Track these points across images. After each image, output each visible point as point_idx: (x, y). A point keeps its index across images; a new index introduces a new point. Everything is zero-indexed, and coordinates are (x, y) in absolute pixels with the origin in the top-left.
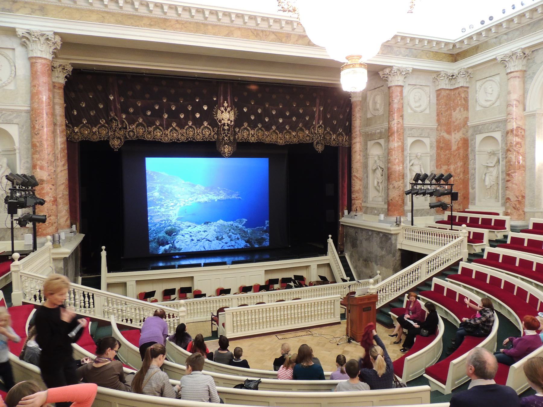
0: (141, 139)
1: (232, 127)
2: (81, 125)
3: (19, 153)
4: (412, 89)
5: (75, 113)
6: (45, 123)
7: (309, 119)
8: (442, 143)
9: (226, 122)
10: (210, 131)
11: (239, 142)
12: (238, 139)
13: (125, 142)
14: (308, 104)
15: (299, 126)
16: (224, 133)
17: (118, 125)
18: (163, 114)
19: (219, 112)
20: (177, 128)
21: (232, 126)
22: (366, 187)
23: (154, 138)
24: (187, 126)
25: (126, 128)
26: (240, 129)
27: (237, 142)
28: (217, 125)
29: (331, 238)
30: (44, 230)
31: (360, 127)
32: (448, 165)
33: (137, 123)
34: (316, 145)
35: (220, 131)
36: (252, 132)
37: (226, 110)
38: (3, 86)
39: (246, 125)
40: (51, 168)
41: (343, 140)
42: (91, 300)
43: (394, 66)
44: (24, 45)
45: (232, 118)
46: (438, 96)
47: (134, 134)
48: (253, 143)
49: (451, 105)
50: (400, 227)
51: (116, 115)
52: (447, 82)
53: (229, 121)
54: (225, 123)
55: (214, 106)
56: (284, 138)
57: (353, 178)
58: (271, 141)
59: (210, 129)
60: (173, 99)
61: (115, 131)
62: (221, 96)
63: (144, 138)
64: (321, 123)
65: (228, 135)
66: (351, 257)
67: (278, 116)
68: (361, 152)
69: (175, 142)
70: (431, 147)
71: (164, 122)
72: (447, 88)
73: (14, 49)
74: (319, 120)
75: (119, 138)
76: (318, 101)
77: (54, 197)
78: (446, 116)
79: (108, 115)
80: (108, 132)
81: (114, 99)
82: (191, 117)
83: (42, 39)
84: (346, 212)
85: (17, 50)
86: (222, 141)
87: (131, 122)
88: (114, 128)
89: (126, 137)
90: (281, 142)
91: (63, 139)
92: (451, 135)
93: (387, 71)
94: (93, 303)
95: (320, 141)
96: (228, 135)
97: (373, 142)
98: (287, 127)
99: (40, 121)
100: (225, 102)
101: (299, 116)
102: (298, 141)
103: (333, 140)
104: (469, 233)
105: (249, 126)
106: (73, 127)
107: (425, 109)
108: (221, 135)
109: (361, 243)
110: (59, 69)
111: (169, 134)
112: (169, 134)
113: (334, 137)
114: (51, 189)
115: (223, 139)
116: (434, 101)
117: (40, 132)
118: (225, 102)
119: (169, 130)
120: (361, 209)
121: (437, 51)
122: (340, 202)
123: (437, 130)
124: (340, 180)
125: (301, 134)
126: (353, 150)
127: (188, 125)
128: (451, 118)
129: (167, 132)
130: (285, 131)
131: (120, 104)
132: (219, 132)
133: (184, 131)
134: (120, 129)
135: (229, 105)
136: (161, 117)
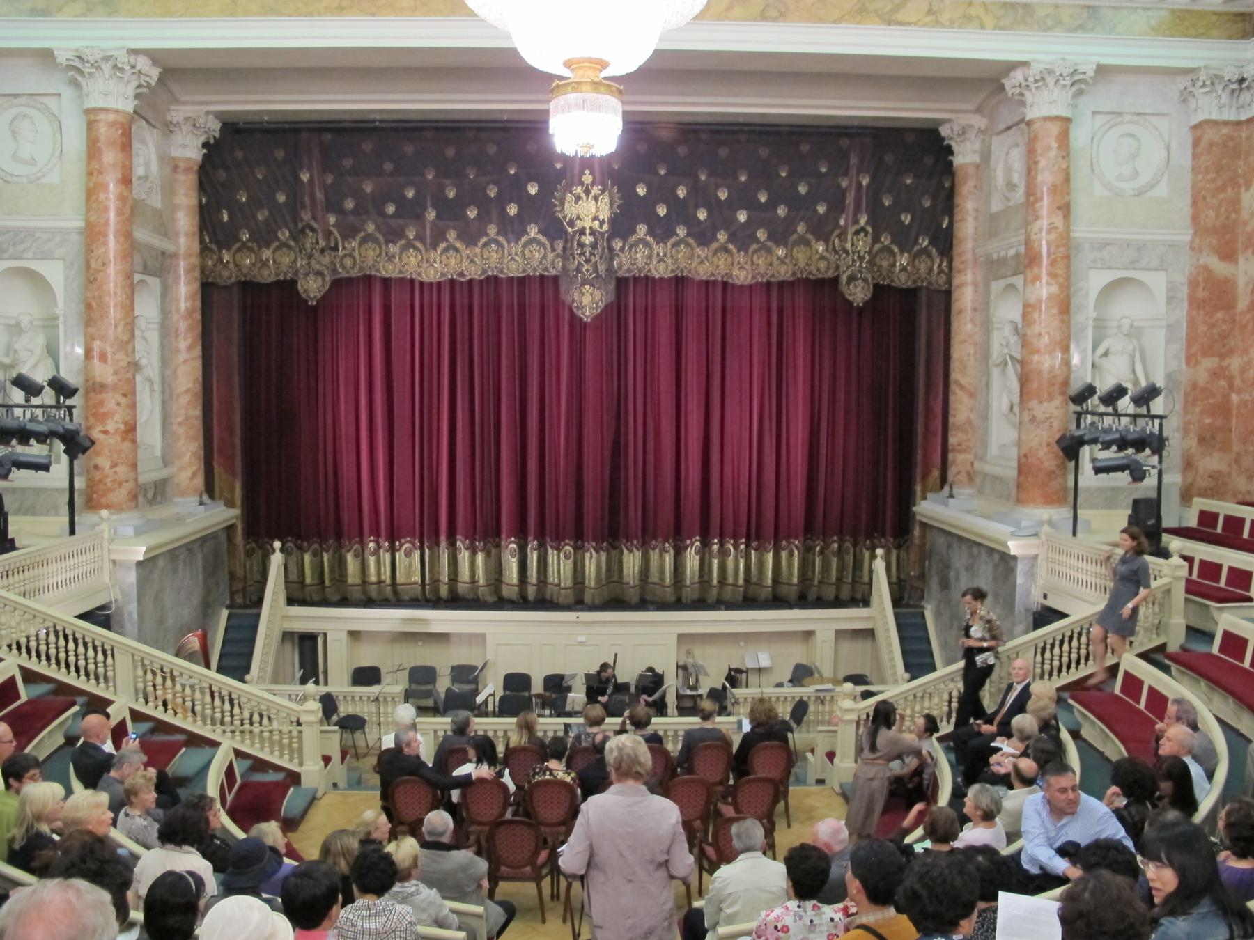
2: (238, 245)
3: (65, 322)
4: (1107, 126)
5: (226, 217)
6: (112, 255)
8: (1201, 288)
10: (545, 249)
12: (620, 268)
15: (795, 231)
17: (317, 242)
18: (425, 208)
20: (458, 245)
21: (602, 234)
23: (400, 272)
25: (336, 249)
30: (103, 495)
32: (1222, 356)
33: (362, 234)
34: (848, 283)
35: (572, 248)
36: (659, 249)
37: (587, 192)
38: (38, 178)
39: (642, 230)
40: (120, 356)
41: (931, 269)
42: (109, 660)
43: (1035, 61)
44: (76, 84)
45: (605, 214)
46: (1196, 143)
47: (355, 263)
48: (661, 279)
49: (1240, 171)
51: (314, 218)
52: (1225, 98)
53: (597, 222)
56: (753, 263)
58: (713, 274)
59: (543, 245)
60: (450, 171)
61: (310, 257)
66: (938, 615)
70: (1170, 299)
71: (428, 231)
72: (1225, 117)
73: (59, 95)
74: (857, 210)
76: (853, 160)
77: (126, 423)
78: (1220, 206)
79: (296, 218)
80: (296, 260)
81: (311, 180)
82: (494, 214)
83: (107, 68)
86: (576, 276)
87: (349, 232)
88: (309, 250)
89: (334, 271)
90: (742, 276)
92: (1236, 262)
93: (1018, 76)
94: (114, 666)
95: (861, 272)
98: (761, 235)
99: (100, 251)
100: (587, 172)
101: (796, 203)
102: (794, 274)
104: (326, 683)
105: (651, 232)
106: (220, 251)
107: (1151, 186)
108: (574, 258)
110: (186, 128)
111: (438, 260)
112: (438, 260)
113: (903, 260)
114: (119, 404)
115: (578, 270)
116: (1184, 159)
117: (99, 276)
121: (1185, 7)
123: (1192, 249)
125: (800, 254)
127: (487, 235)
128: (1237, 211)
131: (325, 190)
132: (568, 252)
133: (478, 250)
134: (322, 251)
136: (419, 217)
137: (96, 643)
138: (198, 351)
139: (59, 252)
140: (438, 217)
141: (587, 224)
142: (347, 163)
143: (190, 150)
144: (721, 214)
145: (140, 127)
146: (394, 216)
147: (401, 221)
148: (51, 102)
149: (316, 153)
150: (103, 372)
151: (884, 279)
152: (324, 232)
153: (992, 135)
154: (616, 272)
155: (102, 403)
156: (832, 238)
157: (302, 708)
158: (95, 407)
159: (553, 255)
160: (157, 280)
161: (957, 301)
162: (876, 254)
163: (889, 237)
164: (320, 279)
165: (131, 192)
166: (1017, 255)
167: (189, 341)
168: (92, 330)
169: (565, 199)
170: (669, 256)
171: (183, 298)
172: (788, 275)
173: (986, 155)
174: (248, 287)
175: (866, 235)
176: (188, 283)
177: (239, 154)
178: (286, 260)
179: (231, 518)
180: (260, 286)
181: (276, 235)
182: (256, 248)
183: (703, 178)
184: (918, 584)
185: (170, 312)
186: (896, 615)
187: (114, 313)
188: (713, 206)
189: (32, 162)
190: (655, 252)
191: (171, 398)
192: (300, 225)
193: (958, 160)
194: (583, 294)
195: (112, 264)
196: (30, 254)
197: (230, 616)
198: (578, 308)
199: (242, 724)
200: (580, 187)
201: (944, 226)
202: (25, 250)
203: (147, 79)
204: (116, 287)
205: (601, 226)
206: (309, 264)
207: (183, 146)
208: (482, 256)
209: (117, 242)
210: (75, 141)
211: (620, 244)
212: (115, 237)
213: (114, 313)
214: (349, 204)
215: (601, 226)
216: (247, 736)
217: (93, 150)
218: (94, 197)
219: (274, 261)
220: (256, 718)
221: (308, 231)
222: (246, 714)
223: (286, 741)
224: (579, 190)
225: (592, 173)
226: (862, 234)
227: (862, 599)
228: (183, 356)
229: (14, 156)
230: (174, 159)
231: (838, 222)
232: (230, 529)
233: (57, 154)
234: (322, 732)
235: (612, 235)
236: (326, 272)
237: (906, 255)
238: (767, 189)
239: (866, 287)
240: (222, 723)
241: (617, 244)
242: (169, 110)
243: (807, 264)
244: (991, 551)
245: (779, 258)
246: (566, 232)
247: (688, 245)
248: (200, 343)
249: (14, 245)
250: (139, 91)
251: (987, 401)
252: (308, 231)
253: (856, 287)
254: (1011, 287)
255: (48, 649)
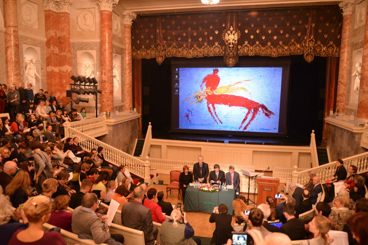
0: (174, 57)
1: (235, 45)
2: (141, 49)
5: (138, 42)
7: (301, 35)
9: (231, 42)
10: (220, 49)
11: (241, 56)
12: (240, 54)
13: (165, 59)
14: (300, 23)
15: (291, 41)
16: (229, 50)
18: (188, 39)
19: (226, 34)
20: (197, 48)
21: (235, 44)
22: (349, 91)
23: (182, 56)
24: (204, 46)
25: (166, 50)
26: (241, 46)
27: (239, 56)
28: (224, 44)
29: (314, 133)
30: (105, 108)
31: (348, 38)
33: (172, 46)
34: (306, 56)
35: (227, 48)
36: (251, 48)
37: (231, 33)
38: (90, 29)
39: (246, 43)
40: (109, 74)
41: (333, 51)
45: (236, 39)
47: (170, 54)
50: (365, 128)
53: (234, 41)
54: (230, 43)
55: (223, 30)
56: (278, 51)
57: (339, 83)
58: (266, 54)
62: (228, 23)
63: (176, 55)
64: (312, 38)
65: (233, 51)
66: (331, 150)
67: (273, 35)
68: (348, 61)
69: (195, 57)
71: (189, 45)
73: (95, 8)
75: (162, 56)
76: (310, 19)
77: (110, 91)
79: (156, 42)
80: (156, 53)
81: (159, 32)
82: (206, 40)
84: (331, 112)
85: (96, 8)
87: (169, 46)
88: (159, 50)
89: (165, 56)
91: (129, 58)
95: (311, 53)
96: (233, 51)
97: (357, 50)
98: (281, 43)
100: (231, 27)
101: (292, 34)
102: (290, 54)
103: (323, 52)
105: (249, 43)
106: (137, 51)
108: (227, 51)
109: (337, 139)
110: (128, 16)
111: (192, 53)
112: (192, 53)
115: (228, 54)
117: (104, 53)
118: (231, 27)
119: (192, 50)
120: (343, 111)
122: (327, 104)
124: (328, 85)
125: (292, 48)
126: (341, 59)
127: (204, 45)
129: (191, 51)
130: (279, 46)
131: (163, 34)
132: (226, 49)
133: (202, 50)
134: (162, 51)
135: (234, 29)
136: (187, 41)
137: (98, 144)
138: (131, 74)
139: (95, 48)
140: (192, 41)
141: (231, 41)
142: (168, 27)
143: (128, 22)
144: (269, 37)
145: (114, 15)
146: (180, 41)
147: (182, 42)
148: (93, 10)
149: (161, 25)
150: (105, 78)
151: (318, 55)
152: (163, 45)
153: (356, 5)
154: (239, 55)
155: (105, 85)
156: (302, 43)
157: (145, 162)
158: (103, 86)
159: (222, 50)
160: (120, 56)
161: (342, 57)
162: (316, 47)
163: (320, 42)
164: (162, 58)
165: (112, 32)
166: (362, 41)
167: (129, 71)
168: (102, 67)
169: (225, 35)
170: (254, 50)
171: (127, 61)
172: (288, 54)
173: (354, 12)
174: (144, 60)
175: (313, 42)
176: (128, 57)
177: (142, 26)
178: (153, 53)
179: (139, 116)
180: (147, 60)
181: (151, 47)
182: (146, 50)
183: (264, 27)
184: (325, 141)
185: (124, 64)
186: (317, 149)
187: (107, 63)
188: (267, 35)
189: (88, 26)
190: (250, 49)
191: (124, 85)
192: (157, 44)
193: (344, 14)
194: (230, 61)
195: (107, 51)
196: (88, 49)
197: (138, 141)
198: (228, 65)
199: (130, 166)
200: (229, 31)
201: (338, 38)
202: (87, 47)
203: (116, 3)
204: (108, 56)
205: (235, 42)
206: (159, 54)
207: (127, 21)
208: (203, 51)
209: (108, 45)
210: (98, 20)
211: (240, 47)
212: (108, 43)
213: (107, 63)
214: (169, 38)
215: (235, 42)
216: (132, 169)
217: (102, 21)
218: (102, 33)
219: (150, 53)
220: (136, 165)
221: (159, 45)
222: (134, 164)
223: (141, 171)
224: (229, 32)
225: (233, 27)
226: (311, 41)
227: (307, 143)
228: (127, 75)
229: (85, 24)
230: (125, 24)
231: (304, 38)
232: (139, 118)
233: (95, 23)
234: (150, 169)
235: (238, 44)
236: (163, 56)
237: (325, 47)
238: (283, 30)
239: (312, 57)
240: (128, 166)
241: (239, 47)
242: (123, 12)
243: (294, 51)
244: (348, 131)
245: (286, 49)
246: (225, 44)
247: (259, 46)
248: (131, 72)
249: (85, 46)
250: (114, 6)
251: (350, 87)
252: (159, 45)
253: (309, 57)
254: (360, 51)
255: (87, 145)
